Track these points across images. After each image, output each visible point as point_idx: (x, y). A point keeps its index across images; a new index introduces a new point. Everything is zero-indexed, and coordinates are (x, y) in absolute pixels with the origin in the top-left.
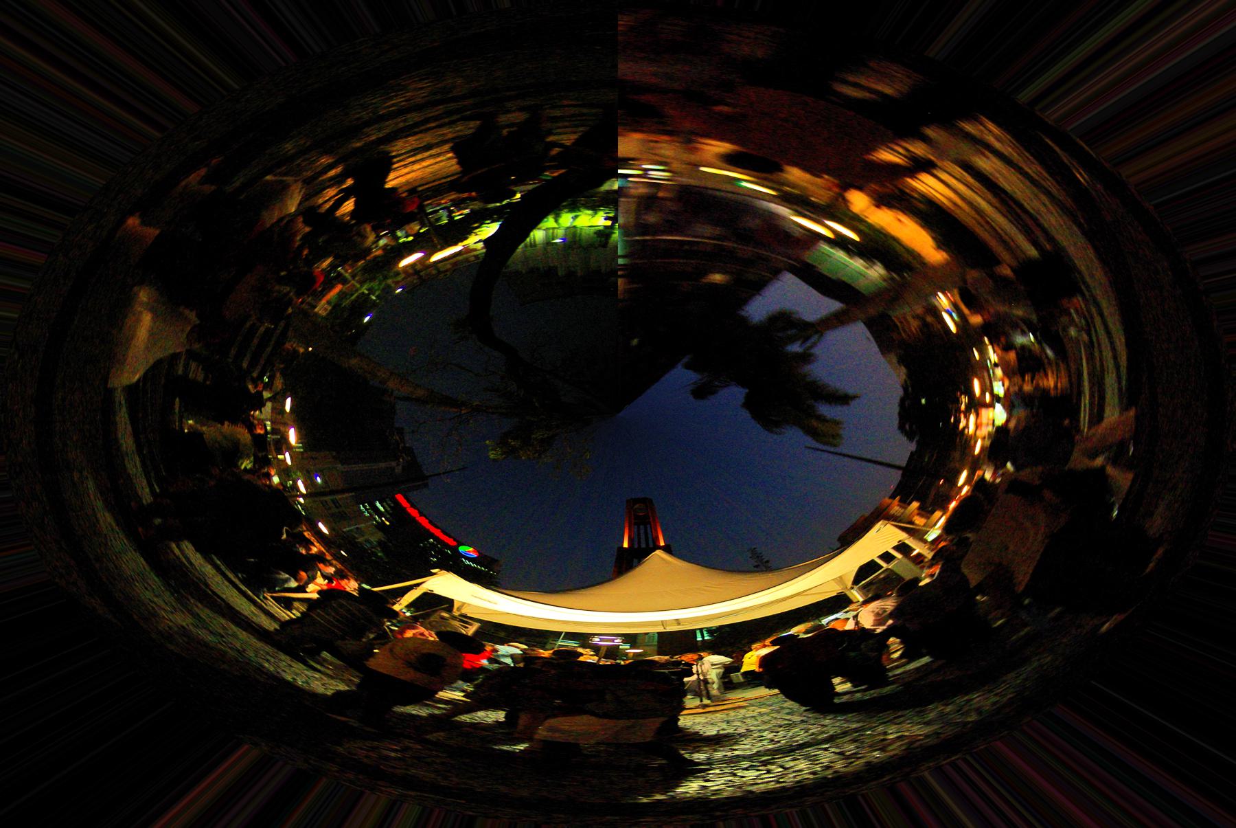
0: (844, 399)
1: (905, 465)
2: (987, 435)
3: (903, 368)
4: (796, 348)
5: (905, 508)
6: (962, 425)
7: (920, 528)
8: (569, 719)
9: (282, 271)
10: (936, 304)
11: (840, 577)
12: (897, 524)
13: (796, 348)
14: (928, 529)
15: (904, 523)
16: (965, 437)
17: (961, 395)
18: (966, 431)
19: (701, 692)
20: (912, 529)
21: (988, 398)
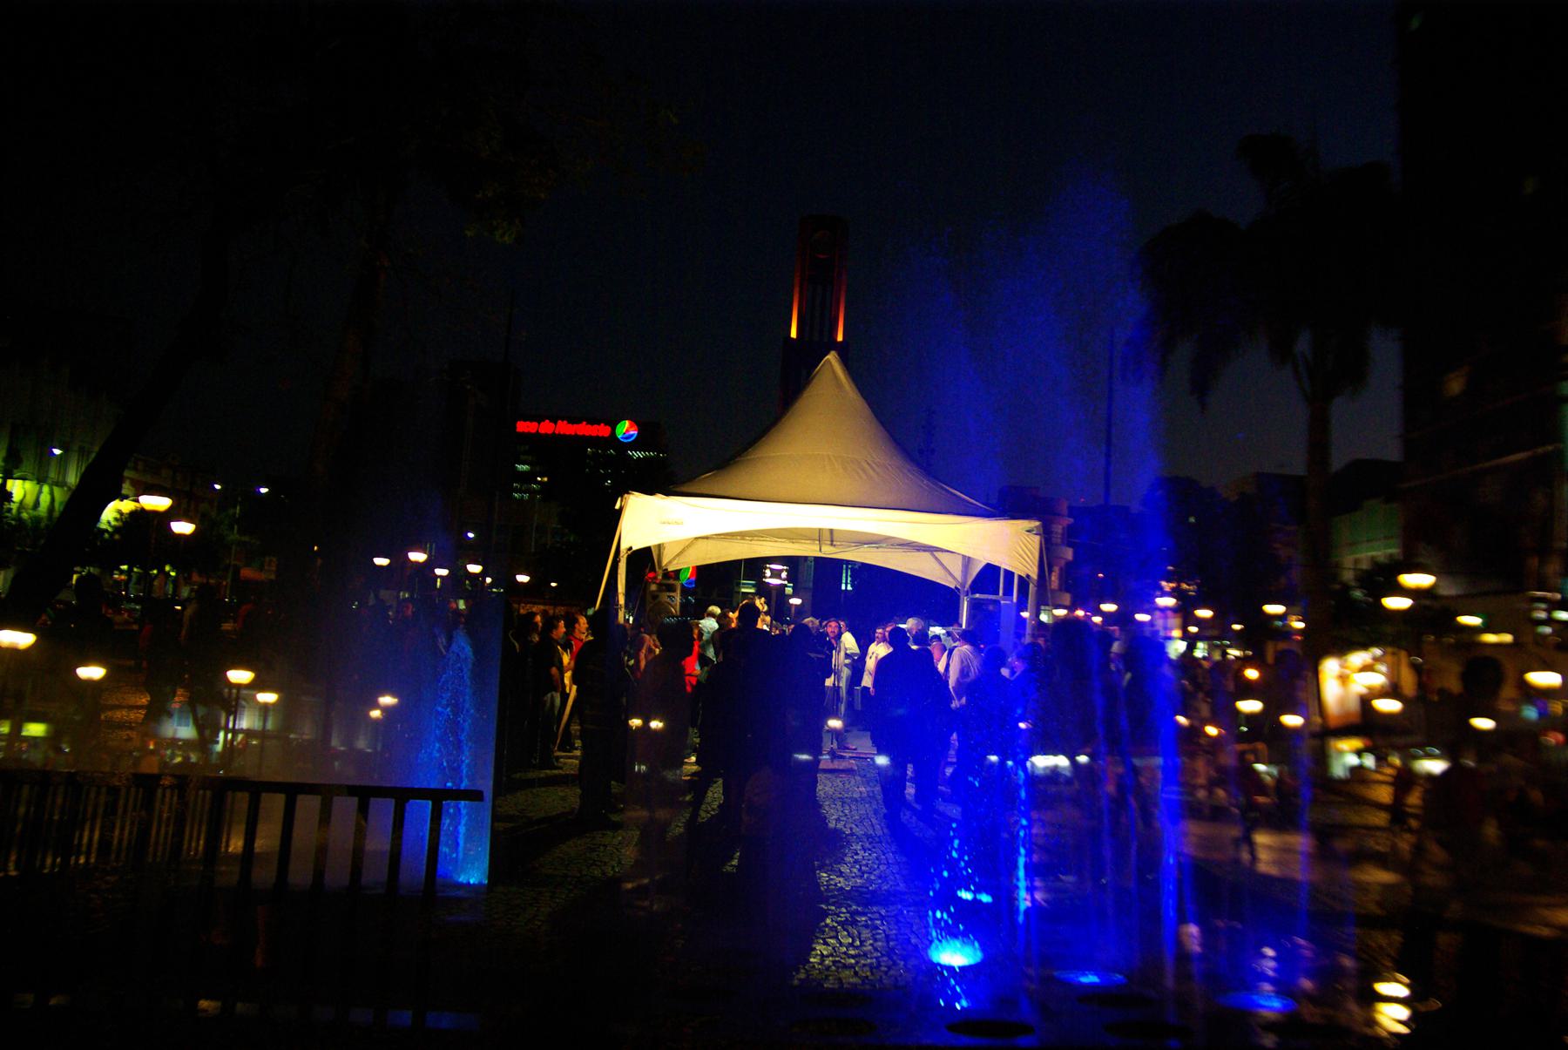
0: (1201, 386)
1: (1112, 504)
2: (1155, 628)
3: (1236, 498)
4: (1303, 344)
5: (1063, 544)
6: (1164, 584)
7: (1048, 588)
8: (496, 713)
9: (178, 610)
10: (1283, 999)
11: (969, 558)
12: (1044, 549)
13: (1303, 344)
14: (1050, 603)
15: (1047, 558)
16: (1152, 592)
17: (1197, 584)
18: (1158, 593)
19: (843, 927)
20: (1045, 576)
21: (1193, 629)
